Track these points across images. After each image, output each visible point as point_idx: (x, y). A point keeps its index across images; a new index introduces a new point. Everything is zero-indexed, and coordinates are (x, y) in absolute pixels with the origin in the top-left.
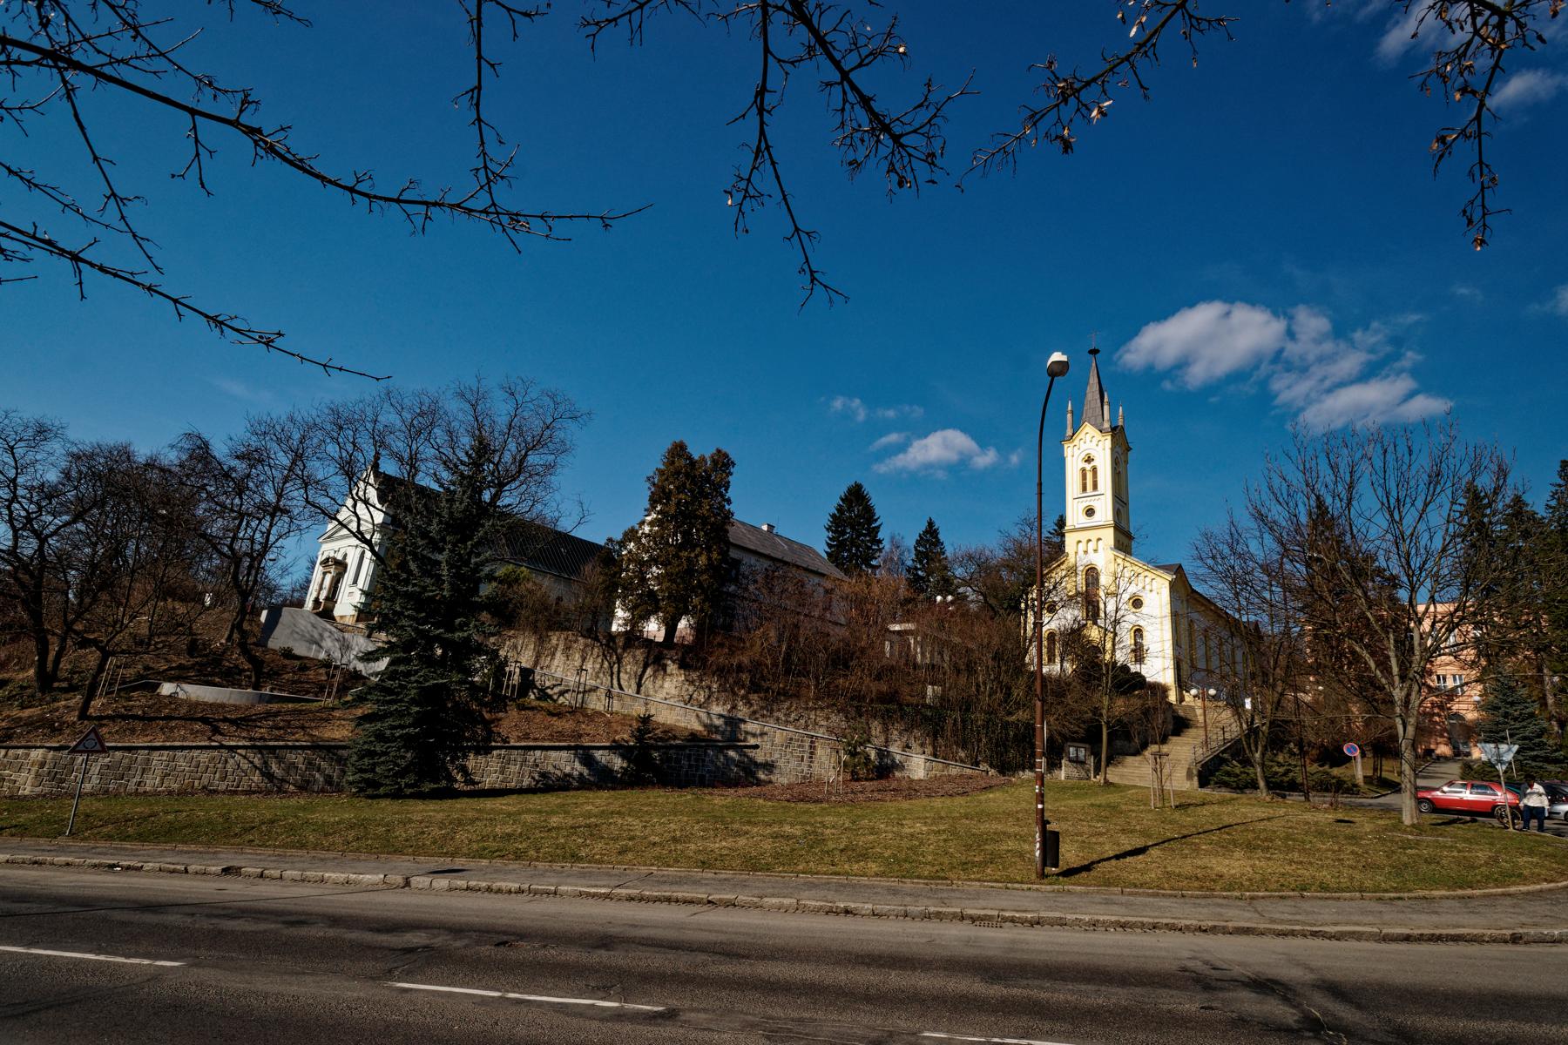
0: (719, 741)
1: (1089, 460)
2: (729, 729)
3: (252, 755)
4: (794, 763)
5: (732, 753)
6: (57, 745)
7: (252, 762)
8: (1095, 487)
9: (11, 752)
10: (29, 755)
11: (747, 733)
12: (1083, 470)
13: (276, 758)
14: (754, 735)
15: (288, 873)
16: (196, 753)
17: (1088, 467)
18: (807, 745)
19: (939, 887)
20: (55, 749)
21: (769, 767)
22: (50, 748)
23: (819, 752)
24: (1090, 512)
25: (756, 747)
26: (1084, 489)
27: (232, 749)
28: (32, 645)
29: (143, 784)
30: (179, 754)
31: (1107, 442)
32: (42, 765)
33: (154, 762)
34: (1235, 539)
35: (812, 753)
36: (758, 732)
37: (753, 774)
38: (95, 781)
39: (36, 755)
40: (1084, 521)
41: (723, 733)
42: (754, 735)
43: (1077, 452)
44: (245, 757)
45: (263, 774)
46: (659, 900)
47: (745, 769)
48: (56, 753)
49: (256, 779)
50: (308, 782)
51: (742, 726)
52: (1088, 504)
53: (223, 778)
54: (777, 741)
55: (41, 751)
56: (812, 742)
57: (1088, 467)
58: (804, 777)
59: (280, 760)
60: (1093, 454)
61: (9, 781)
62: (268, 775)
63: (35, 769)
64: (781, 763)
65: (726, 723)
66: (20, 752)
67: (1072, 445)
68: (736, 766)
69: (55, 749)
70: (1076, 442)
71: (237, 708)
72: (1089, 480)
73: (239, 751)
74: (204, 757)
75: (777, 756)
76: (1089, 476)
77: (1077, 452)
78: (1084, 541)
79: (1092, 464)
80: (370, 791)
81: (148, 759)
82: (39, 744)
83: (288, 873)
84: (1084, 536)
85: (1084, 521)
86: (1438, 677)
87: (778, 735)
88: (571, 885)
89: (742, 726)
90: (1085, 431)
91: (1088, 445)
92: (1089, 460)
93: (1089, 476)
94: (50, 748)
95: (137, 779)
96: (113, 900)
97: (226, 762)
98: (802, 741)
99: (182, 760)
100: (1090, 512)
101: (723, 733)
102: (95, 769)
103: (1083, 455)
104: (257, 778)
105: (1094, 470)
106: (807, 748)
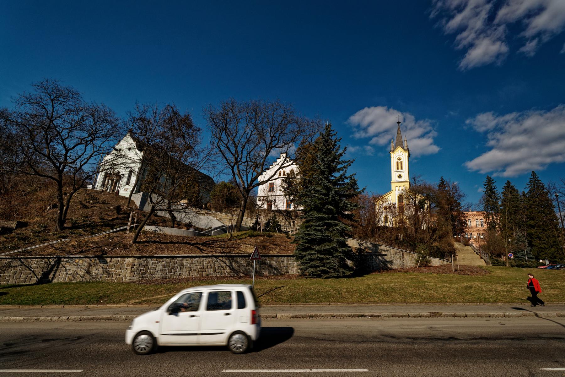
0: (371, 253)
1: (399, 159)
2: (374, 248)
3: (225, 260)
4: (398, 261)
5: (380, 257)
6: (140, 256)
7: (225, 263)
8: (402, 168)
9: (114, 259)
10: (124, 261)
11: (381, 250)
12: (397, 162)
13: (235, 261)
14: (384, 251)
15: (42, 318)
16: (202, 259)
17: (399, 161)
18: (401, 254)
19: (298, 306)
20: (139, 258)
21: (391, 262)
22: (136, 257)
23: (405, 257)
24: (400, 177)
25: (386, 255)
26: (398, 169)
27: (217, 257)
28: (131, 199)
29: (181, 275)
30: (195, 260)
31: (406, 154)
32: (133, 266)
33: (185, 264)
34: (358, 189)
35: (403, 257)
36: (386, 249)
37: (386, 265)
38: (159, 273)
39: (129, 261)
40: (398, 180)
41: (372, 250)
42: (384, 251)
43: (395, 156)
44: (222, 261)
45: (230, 269)
46: (349, 316)
47: (384, 263)
48: (139, 260)
49: (228, 271)
50: (248, 272)
51: (379, 247)
52: (399, 174)
53: (215, 271)
54: (392, 252)
55: (131, 259)
56: (403, 253)
57: (399, 161)
58: (402, 266)
59: (236, 262)
60: (401, 157)
61: (116, 274)
62: (232, 269)
63: (129, 268)
64: (394, 261)
65: (373, 246)
66: (119, 259)
67: (393, 154)
68: (382, 262)
69: (139, 258)
70: (395, 153)
71: (184, 237)
72: (400, 166)
73: (220, 258)
74: (206, 261)
75: (393, 258)
76: (399, 165)
77: (395, 156)
78: (398, 186)
79: (401, 161)
80: (324, 276)
81: (182, 263)
82: (130, 255)
83: (42, 318)
84: (398, 184)
85: (398, 180)
86: (470, 234)
87: (392, 250)
88: (328, 313)
89: (379, 247)
90: (398, 149)
91: (400, 154)
92: (399, 159)
93: (399, 165)
94: (136, 257)
95: (178, 272)
96: (312, 335)
97: (215, 263)
98: (400, 253)
99: (196, 263)
100: (400, 177)
101: (372, 250)
102: (159, 268)
103: (397, 157)
104: (228, 270)
105: (401, 163)
106: (401, 255)
